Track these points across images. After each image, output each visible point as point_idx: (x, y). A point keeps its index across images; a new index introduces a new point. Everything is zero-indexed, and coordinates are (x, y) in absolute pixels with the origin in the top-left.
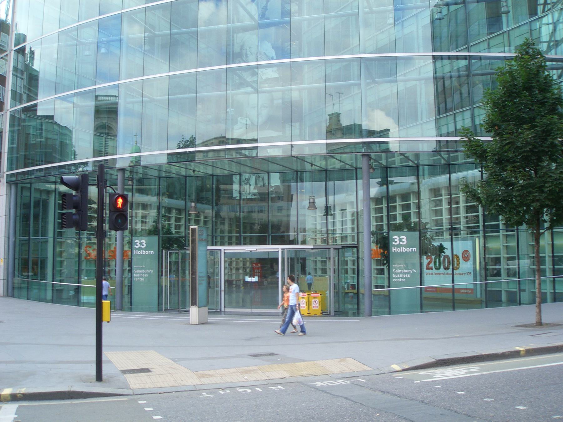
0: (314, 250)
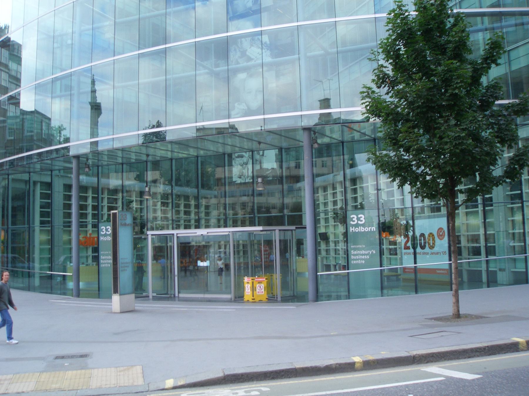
0: (263, 233)
